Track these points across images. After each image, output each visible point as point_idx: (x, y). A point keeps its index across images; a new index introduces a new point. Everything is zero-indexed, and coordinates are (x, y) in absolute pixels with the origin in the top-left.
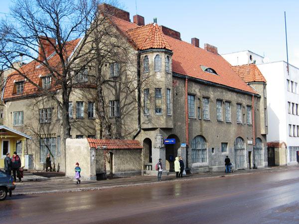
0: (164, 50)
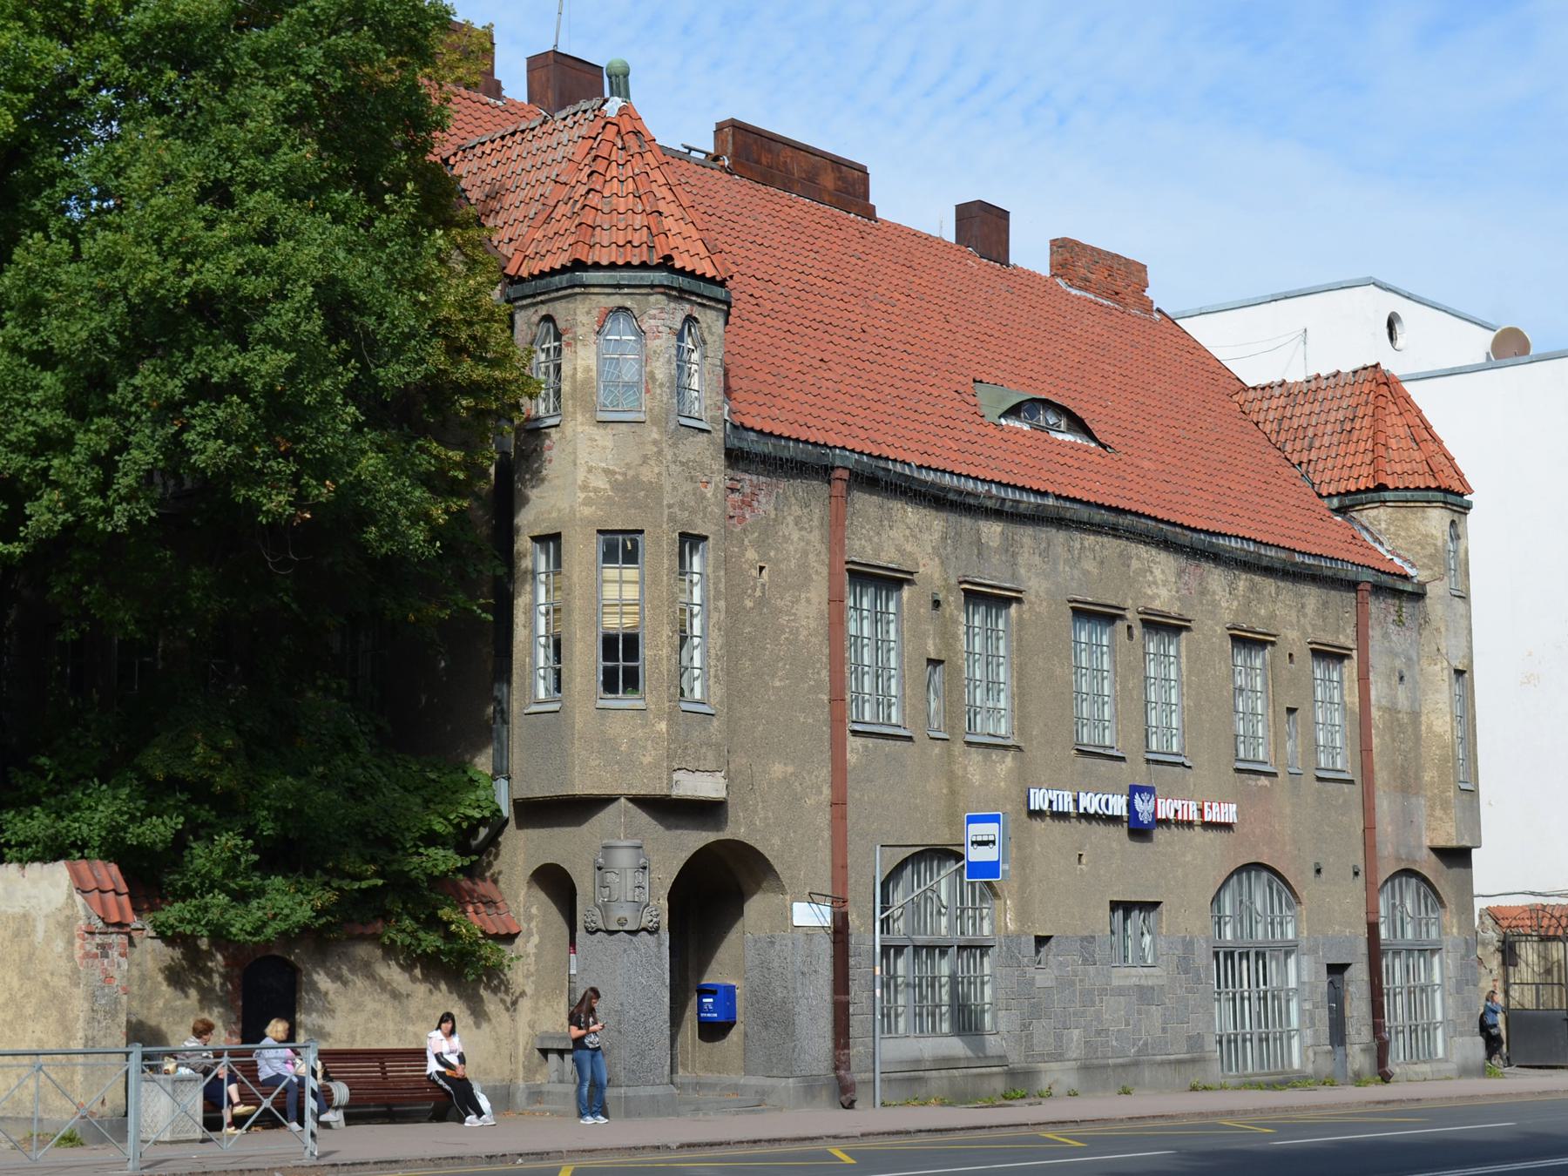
0: (660, 277)
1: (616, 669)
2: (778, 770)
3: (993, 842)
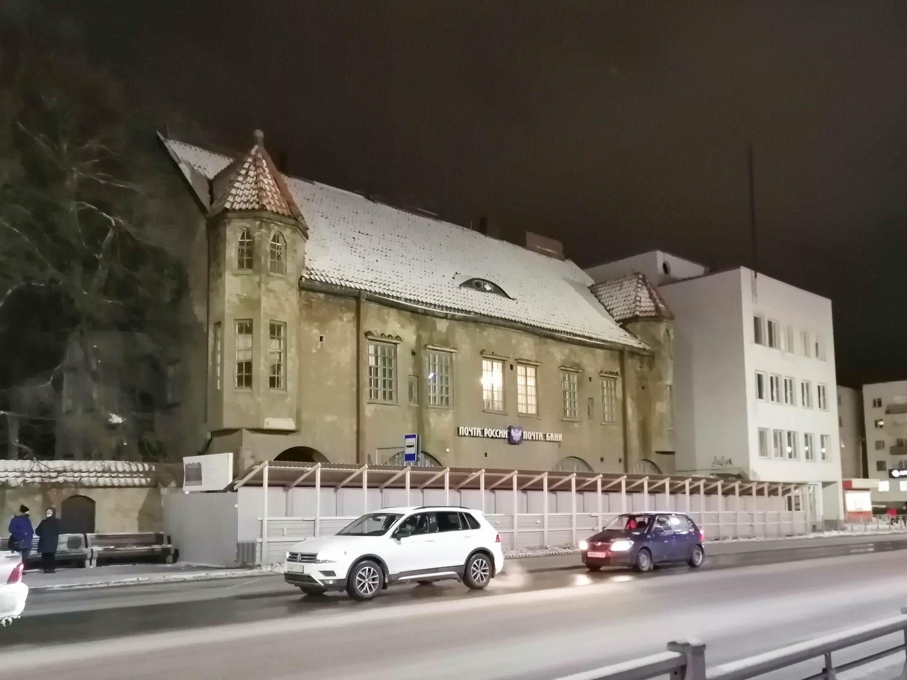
1: (242, 376)
2: (329, 418)
3: (413, 446)
